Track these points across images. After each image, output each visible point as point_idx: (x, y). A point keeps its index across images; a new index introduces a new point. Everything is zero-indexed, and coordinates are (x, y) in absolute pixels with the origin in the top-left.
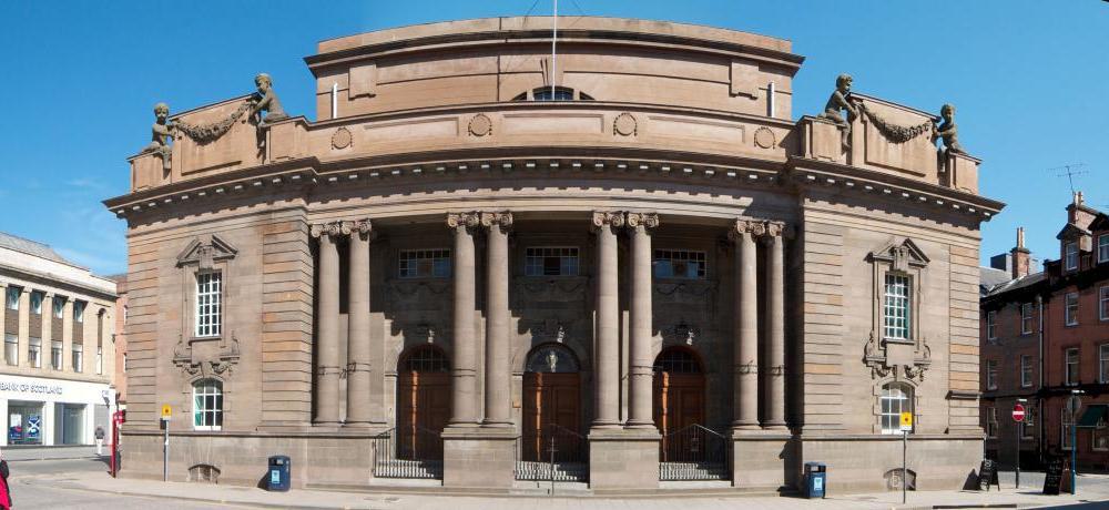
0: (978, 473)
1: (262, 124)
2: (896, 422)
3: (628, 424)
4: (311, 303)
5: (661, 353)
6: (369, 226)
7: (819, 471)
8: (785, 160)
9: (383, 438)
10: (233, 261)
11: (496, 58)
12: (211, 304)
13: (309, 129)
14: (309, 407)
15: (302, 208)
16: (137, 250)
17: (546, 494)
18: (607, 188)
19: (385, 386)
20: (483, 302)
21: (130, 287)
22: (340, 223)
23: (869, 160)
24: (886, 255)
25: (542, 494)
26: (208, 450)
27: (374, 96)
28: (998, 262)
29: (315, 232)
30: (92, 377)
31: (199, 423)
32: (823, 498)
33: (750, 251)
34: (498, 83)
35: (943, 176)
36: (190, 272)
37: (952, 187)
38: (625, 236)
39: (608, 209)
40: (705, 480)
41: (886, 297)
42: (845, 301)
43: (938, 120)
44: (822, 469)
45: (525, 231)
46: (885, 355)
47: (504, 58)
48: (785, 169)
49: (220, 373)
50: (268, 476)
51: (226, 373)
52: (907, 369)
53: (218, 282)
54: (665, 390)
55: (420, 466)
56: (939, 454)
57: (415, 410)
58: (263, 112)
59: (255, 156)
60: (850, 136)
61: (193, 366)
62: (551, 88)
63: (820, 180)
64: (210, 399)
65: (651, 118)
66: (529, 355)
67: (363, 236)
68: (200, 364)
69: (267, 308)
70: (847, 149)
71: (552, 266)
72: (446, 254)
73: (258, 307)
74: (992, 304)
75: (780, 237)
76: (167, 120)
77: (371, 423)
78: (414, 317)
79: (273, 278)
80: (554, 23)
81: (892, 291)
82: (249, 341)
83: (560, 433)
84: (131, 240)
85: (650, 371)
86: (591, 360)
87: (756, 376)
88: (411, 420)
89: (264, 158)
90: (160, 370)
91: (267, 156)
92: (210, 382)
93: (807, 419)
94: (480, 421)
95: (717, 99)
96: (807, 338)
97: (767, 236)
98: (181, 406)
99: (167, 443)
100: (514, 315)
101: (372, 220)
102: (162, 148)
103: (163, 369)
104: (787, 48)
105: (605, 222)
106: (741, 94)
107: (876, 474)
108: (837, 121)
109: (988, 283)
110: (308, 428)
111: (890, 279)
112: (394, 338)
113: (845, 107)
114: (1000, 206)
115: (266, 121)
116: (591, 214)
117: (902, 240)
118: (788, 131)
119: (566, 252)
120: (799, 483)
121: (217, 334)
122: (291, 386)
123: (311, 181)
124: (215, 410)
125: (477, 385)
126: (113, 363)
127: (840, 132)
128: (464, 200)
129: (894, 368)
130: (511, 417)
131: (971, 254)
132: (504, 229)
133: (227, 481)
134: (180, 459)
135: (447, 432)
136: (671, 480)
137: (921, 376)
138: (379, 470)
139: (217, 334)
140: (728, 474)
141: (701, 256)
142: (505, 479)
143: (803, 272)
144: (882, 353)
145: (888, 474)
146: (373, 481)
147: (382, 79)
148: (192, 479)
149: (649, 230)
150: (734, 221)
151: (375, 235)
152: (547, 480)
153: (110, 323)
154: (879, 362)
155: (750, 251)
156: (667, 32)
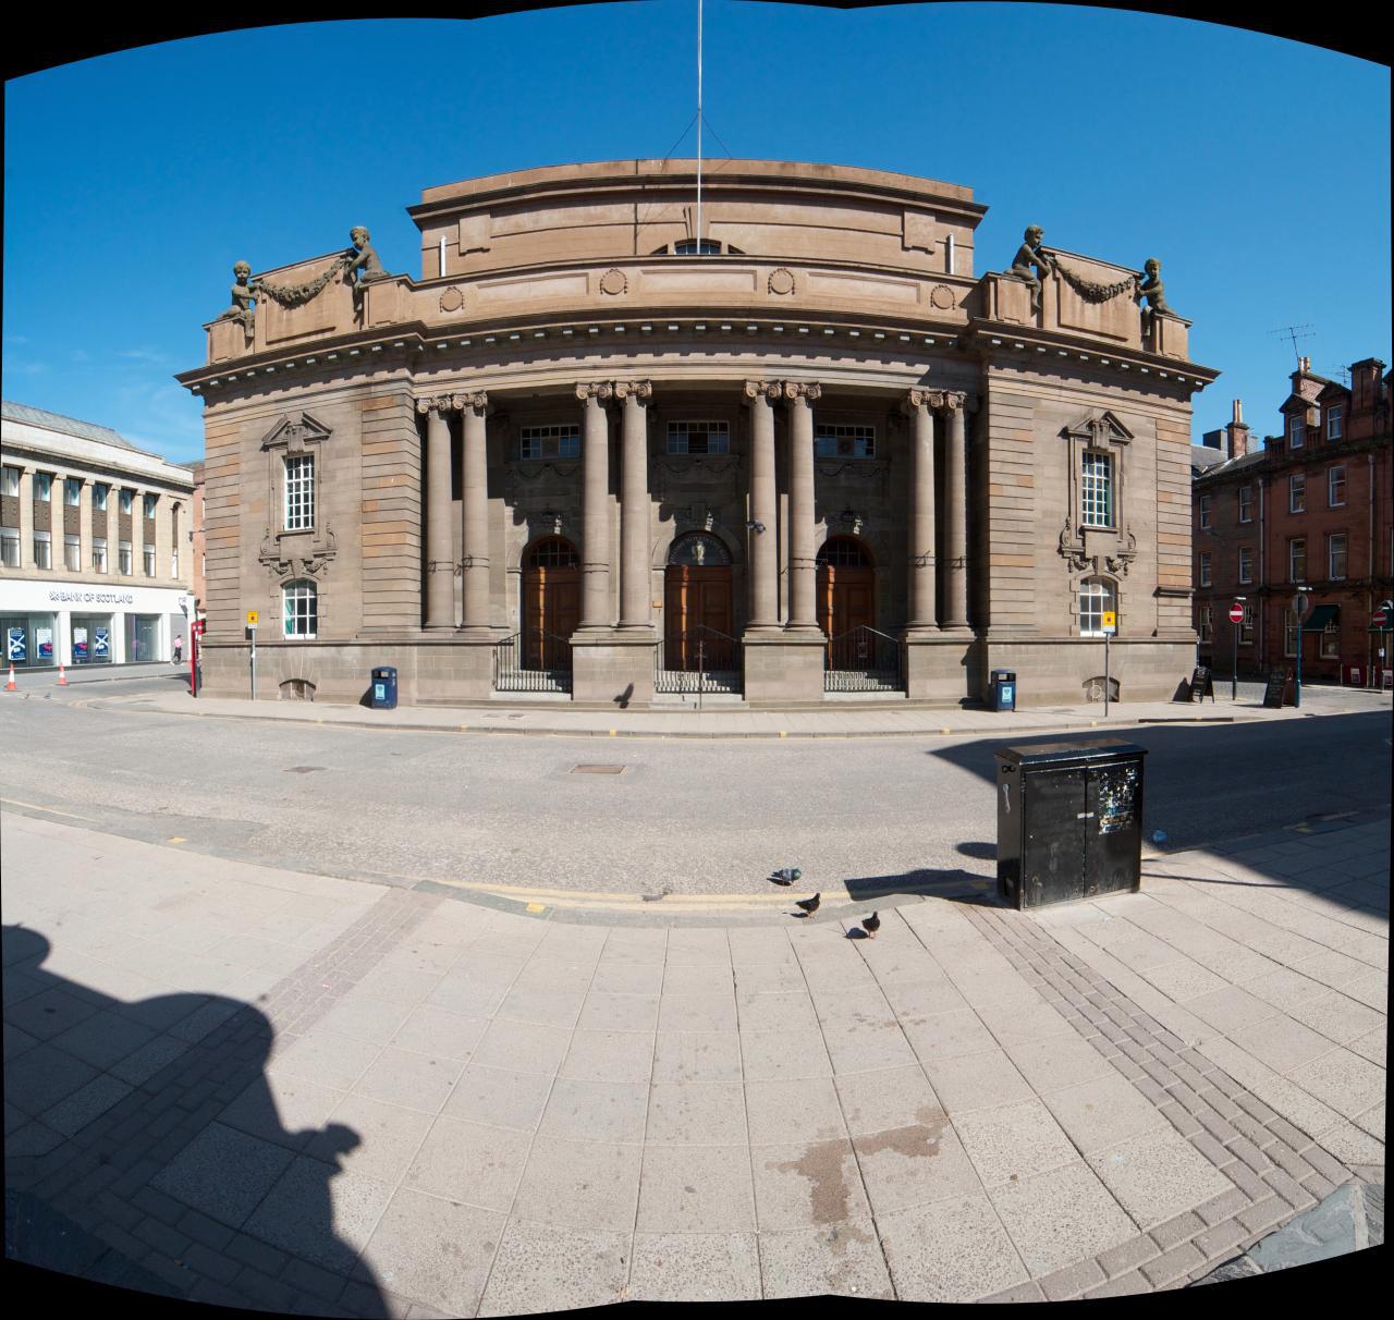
0: (1189, 682)
1: (359, 284)
2: (1097, 623)
3: (788, 626)
9: (505, 644)
11: (633, 205)
12: (302, 493)
13: (413, 289)
15: (407, 379)
16: (216, 432)
18: (761, 354)
19: (507, 585)
20: (617, 484)
22: (451, 396)
23: (1062, 322)
24: (1084, 430)
26: (302, 661)
27: (488, 250)
28: (1212, 439)
29: (422, 408)
31: (290, 631)
35: (1148, 341)
36: (277, 456)
37: (1159, 353)
41: (1084, 479)
42: (1037, 483)
43: (1141, 277)
44: (1011, 678)
45: (665, 403)
46: (1084, 545)
48: (967, 332)
50: (371, 691)
51: (320, 572)
52: (1109, 561)
53: (310, 466)
54: (831, 586)
56: (1146, 660)
57: (542, 612)
58: (359, 270)
61: (282, 565)
62: (696, 240)
63: (1007, 345)
64: (302, 603)
65: (811, 274)
66: (673, 545)
67: (478, 411)
68: (290, 562)
69: (367, 495)
70: (1038, 310)
71: (698, 442)
72: (575, 431)
73: (358, 495)
74: (1206, 488)
76: (249, 280)
78: (538, 504)
80: (698, 167)
81: (1091, 472)
84: (209, 420)
85: (813, 564)
87: (933, 569)
88: (539, 625)
89: (362, 323)
90: (244, 570)
93: (994, 618)
96: (993, 525)
99: (253, 656)
100: (654, 500)
101: (488, 393)
103: (247, 569)
104: (967, 196)
105: (759, 393)
106: (915, 248)
107: (1074, 684)
108: (1025, 278)
109: (1200, 463)
110: (417, 634)
111: (1088, 458)
112: (517, 528)
113: (1034, 263)
115: (365, 281)
116: (743, 383)
117: (1102, 413)
119: (713, 427)
122: (397, 586)
123: (417, 349)
125: (611, 582)
127: (1029, 291)
128: (595, 367)
129: (1095, 560)
130: (650, 618)
131: (1181, 429)
132: (641, 400)
133: (325, 698)
134: (268, 674)
135: (576, 638)
137: (1126, 570)
141: (870, 432)
143: (987, 449)
145: (1088, 683)
147: (496, 231)
148: (283, 697)
149: (810, 402)
150: (908, 392)
151: (492, 411)
153: (186, 520)
154: (1077, 553)
156: (828, 176)
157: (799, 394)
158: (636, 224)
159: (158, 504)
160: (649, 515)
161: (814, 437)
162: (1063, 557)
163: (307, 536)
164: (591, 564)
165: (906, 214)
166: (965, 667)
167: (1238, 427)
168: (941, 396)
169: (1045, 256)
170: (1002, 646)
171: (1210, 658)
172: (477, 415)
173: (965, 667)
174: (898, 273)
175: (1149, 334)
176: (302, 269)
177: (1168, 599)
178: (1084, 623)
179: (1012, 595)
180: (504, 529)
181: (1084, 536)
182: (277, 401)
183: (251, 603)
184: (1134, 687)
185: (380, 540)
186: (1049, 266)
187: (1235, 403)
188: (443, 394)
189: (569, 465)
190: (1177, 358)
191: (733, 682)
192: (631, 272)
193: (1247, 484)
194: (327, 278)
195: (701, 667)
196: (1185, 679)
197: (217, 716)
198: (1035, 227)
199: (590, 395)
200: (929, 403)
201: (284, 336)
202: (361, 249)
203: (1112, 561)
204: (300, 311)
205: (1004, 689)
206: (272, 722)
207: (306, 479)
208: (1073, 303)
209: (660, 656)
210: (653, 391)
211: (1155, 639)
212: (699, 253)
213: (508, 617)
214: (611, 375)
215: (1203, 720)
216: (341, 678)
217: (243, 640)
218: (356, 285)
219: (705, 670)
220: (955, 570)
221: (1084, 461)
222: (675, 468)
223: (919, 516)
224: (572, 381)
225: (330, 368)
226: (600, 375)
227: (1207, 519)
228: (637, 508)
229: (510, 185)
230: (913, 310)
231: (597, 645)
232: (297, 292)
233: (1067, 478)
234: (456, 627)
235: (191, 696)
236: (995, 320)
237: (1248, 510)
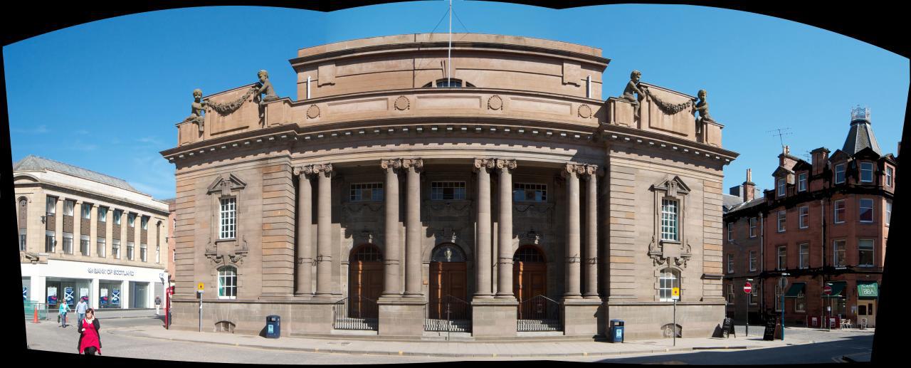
0: (721, 326)
1: (262, 102)
2: (669, 294)
3: (497, 295)
8: (597, 126)
9: (340, 304)
11: (412, 60)
12: (229, 218)
13: (292, 106)
14: (292, 284)
15: (288, 156)
18: (483, 143)
19: (341, 270)
20: (404, 217)
21: (177, 207)
22: (312, 166)
23: (651, 126)
24: (663, 186)
25: (442, 340)
26: (228, 311)
27: (334, 84)
29: (296, 172)
30: (153, 265)
31: (222, 294)
33: (575, 184)
34: (414, 77)
35: (699, 136)
36: (216, 197)
37: (705, 143)
38: (495, 174)
40: (546, 331)
41: (663, 214)
42: (636, 216)
43: (696, 100)
44: (622, 324)
45: (431, 171)
46: (662, 251)
47: (417, 60)
48: (598, 131)
50: (266, 328)
52: (676, 260)
53: (234, 204)
54: (521, 273)
55: (364, 322)
56: (697, 314)
57: (360, 286)
61: (218, 258)
63: (620, 138)
64: (229, 279)
65: (512, 99)
66: (434, 251)
67: (327, 175)
68: (222, 256)
69: (265, 220)
70: (638, 119)
71: (448, 193)
72: (380, 186)
73: (260, 220)
74: (730, 218)
75: (595, 175)
77: (332, 294)
79: (269, 201)
80: (449, 37)
81: (667, 210)
82: (253, 242)
85: (511, 261)
86: (473, 254)
87: (579, 264)
89: (264, 124)
90: (197, 260)
91: (266, 123)
92: (229, 268)
93: (612, 292)
94: (402, 293)
96: (612, 240)
97: (586, 175)
98: (210, 283)
99: (201, 307)
100: (424, 225)
101: (333, 164)
103: (199, 260)
104: (599, 54)
105: (482, 165)
106: (569, 83)
107: (656, 327)
108: (631, 100)
109: (728, 204)
110: (292, 298)
111: (665, 202)
112: (347, 240)
113: (636, 92)
115: (265, 101)
116: (473, 160)
117: (673, 177)
119: (457, 184)
121: (233, 237)
122: (281, 271)
123: (293, 139)
125: (400, 270)
126: (166, 256)
128: (392, 151)
129: (668, 259)
130: (421, 289)
131: (717, 186)
132: (417, 170)
133: (240, 332)
134: (209, 317)
136: (525, 331)
138: (337, 325)
139: (233, 237)
140: (561, 327)
141: (544, 187)
142: (418, 330)
143: (609, 198)
144: (660, 249)
145: (664, 327)
146: (333, 332)
148: (217, 330)
149: (511, 170)
150: (565, 165)
151: (335, 174)
152: (445, 331)
155: (575, 184)
156: (522, 43)
159: (149, 222)
175: (700, 132)
177: (709, 280)
180: (340, 240)
185: (272, 245)
201: (220, 131)
208: (658, 114)
212: (449, 86)
216: (249, 320)
218: (261, 103)
219: (451, 319)
220: (591, 265)
222: (436, 208)
223: (571, 235)
232: (228, 107)
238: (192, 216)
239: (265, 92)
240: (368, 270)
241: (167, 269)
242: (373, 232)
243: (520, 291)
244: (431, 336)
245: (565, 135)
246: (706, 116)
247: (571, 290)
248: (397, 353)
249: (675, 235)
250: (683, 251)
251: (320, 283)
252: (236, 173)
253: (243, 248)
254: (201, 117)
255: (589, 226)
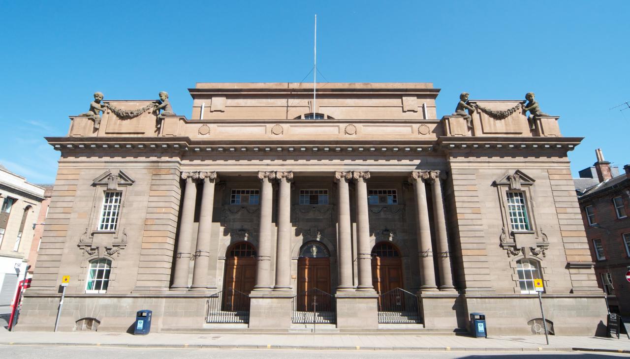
0: (605, 323)
1: (160, 116)
2: (530, 286)
3: (358, 288)
4: (177, 215)
5: (375, 246)
6: (215, 176)
7: (480, 319)
8: (436, 139)
9: (214, 297)
10: (131, 187)
11: (286, 100)
12: (112, 211)
13: (186, 123)
14: (169, 278)
15: (178, 162)
16: (65, 172)
17: (311, 332)
18: (342, 160)
19: (218, 265)
20: (276, 218)
21: (54, 194)
22: (199, 172)
23: (485, 132)
24: (505, 181)
25: (307, 332)
26: (92, 307)
27: (223, 112)
28: (585, 173)
29: (184, 176)
30: (9, 253)
31: (90, 288)
32: (486, 337)
33: (422, 188)
34: (287, 111)
35: (535, 131)
36: (100, 190)
37: (542, 136)
38: (353, 184)
39: (343, 170)
40: (406, 323)
41: (509, 206)
42: (482, 211)
43: (524, 102)
44: (482, 318)
45: (299, 182)
46: (515, 241)
47: (290, 100)
48: (437, 143)
49: (110, 254)
50: (135, 324)
51: (115, 255)
52: (532, 249)
53: (119, 198)
54: (378, 267)
55: (235, 315)
56: (570, 308)
57: (234, 280)
58: (161, 110)
59: (154, 132)
60: (472, 122)
61: (92, 249)
62: (313, 114)
63: (458, 147)
64: (101, 272)
65: (364, 126)
66: (301, 248)
67: (211, 180)
68: (98, 248)
69: (149, 216)
70: (471, 128)
71: (314, 199)
72: (257, 192)
73: (144, 215)
74: (587, 201)
75: (438, 179)
76: (102, 102)
77: (207, 288)
78: (237, 225)
79: (155, 199)
80: (314, 86)
81: (513, 202)
82: (134, 236)
83: (319, 294)
84: (61, 164)
85: (369, 256)
86: (336, 250)
87: (432, 258)
88: (232, 287)
89: (159, 133)
90: (66, 251)
91: (161, 132)
92: (103, 260)
93: (468, 284)
94: (273, 287)
95: (398, 115)
96: (461, 234)
97: (430, 179)
98: (78, 276)
99: (61, 303)
100: (293, 226)
101: (217, 172)
102: (95, 116)
103: (69, 251)
104: (431, 86)
105: (342, 177)
106: (408, 111)
107: (522, 322)
108: (463, 115)
109: (581, 188)
110: (166, 291)
111: (510, 195)
112: (225, 237)
113: (466, 108)
114: (580, 140)
115: (163, 115)
116: (334, 173)
117: (514, 171)
118: (436, 125)
119: (321, 192)
120: (468, 327)
121: (113, 230)
122: (158, 265)
123: (185, 149)
124: (103, 279)
125: (271, 265)
126: (30, 244)
127: (466, 120)
128: (268, 165)
129: (523, 249)
130: (290, 284)
131: (565, 172)
132: (288, 180)
133: (105, 329)
134: (69, 314)
135: (253, 294)
136: (386, 323)
137: (544, 254)
138: (210, 319)
139: (113, 230)
140: (420, 320)
141: (394, 192)
142: (287, 323)
143: (454, 196)
144: (512, 240)
145: (531, 322)
146: (206, 326)
147: (228, 104)
148: (77, 329)
149: (365, 180)
150: (411, 173)
151: (218, 181)
152: (311, 323)
153: (33, 216)
154: (511, 246)
155: (422, 188)
156: (369, 87)
157: (360, 177)
158: (288, 107)
159: (15, 205)
160: (291, 233)
161: (368, 196)
162: (503, 249)
163: (111, 234)
164: (262, 256)
165: (403, 98)
166: (455, 311)
167: (602, 163)
168: (427, 173)
169: (471, 104)
170: (474, 299)
171: (617, 306)
172: (211, 182)
173: (455, 311)
174: (404, 123)
175: (534, 127)
176: (132, 103)
177: (577, 270)
178: (522, 285)
179: (477, 271)
180: (218, 237)
181: (514, 236)
182: (105, 162)
183: (65, 270)
184: (563, 326)
185: (152, 240)
186: (474, 108)
187: (597, 152)
188: (195, 171)
189: (253, 208)
190: (554, 136)
191: (331, 318)
192: (285, 126)
193: (619, 195)
194: (144, 110)
195: (315, 310)
196: (601, 321)
197: (23, 344)
198: (464, 93)
199: (265, 177)
200: (422, 177)
201: (116, 131)
202: (163, 101)
203: (534, 249)
204: (127, 122)
205: (479, 324)
206: (65, 346)
207: (116, 204)
208: (489, 121)
209: (295, 304)
210: (294, 176)
211: (572, 295)
212: (314, 118)
213: (216, 282)
214: (275, 168)
215: (624, 352)
216: (118, 316)
217: (56, 293)
218: (159, 116)
219: (317, 311)
220: (444, 258)
221: (508, 197)
222: (303, 211)
223: (422, 231)
224: (257, 170)
225: (138, 151)
226: (270, 168)
227: (593, 219)
228: (285, 230)
229: (236, 88)
230: (411, 137)
231: (263, 298)
232: (127, 113)
233: (499, 206)
234: (188, 288)
235: (7, 331)
236: (450, 136)
237: (623, 211)
238: (70, 205)
239: (164, 108)
240: (242, 265)
241: (27, 258)
242: (248, 230)
243: (379, 284)
244: (300, 328)
245: (409, 149)
246: (538, 113)
247: (427, 282)
248: (265, 347)
249: (526, 226)
250: (538, 240)
251: (197, 277)
252: (124, 170)
253: (122, 241)
254: (99, 116)
255: (438, 223)
